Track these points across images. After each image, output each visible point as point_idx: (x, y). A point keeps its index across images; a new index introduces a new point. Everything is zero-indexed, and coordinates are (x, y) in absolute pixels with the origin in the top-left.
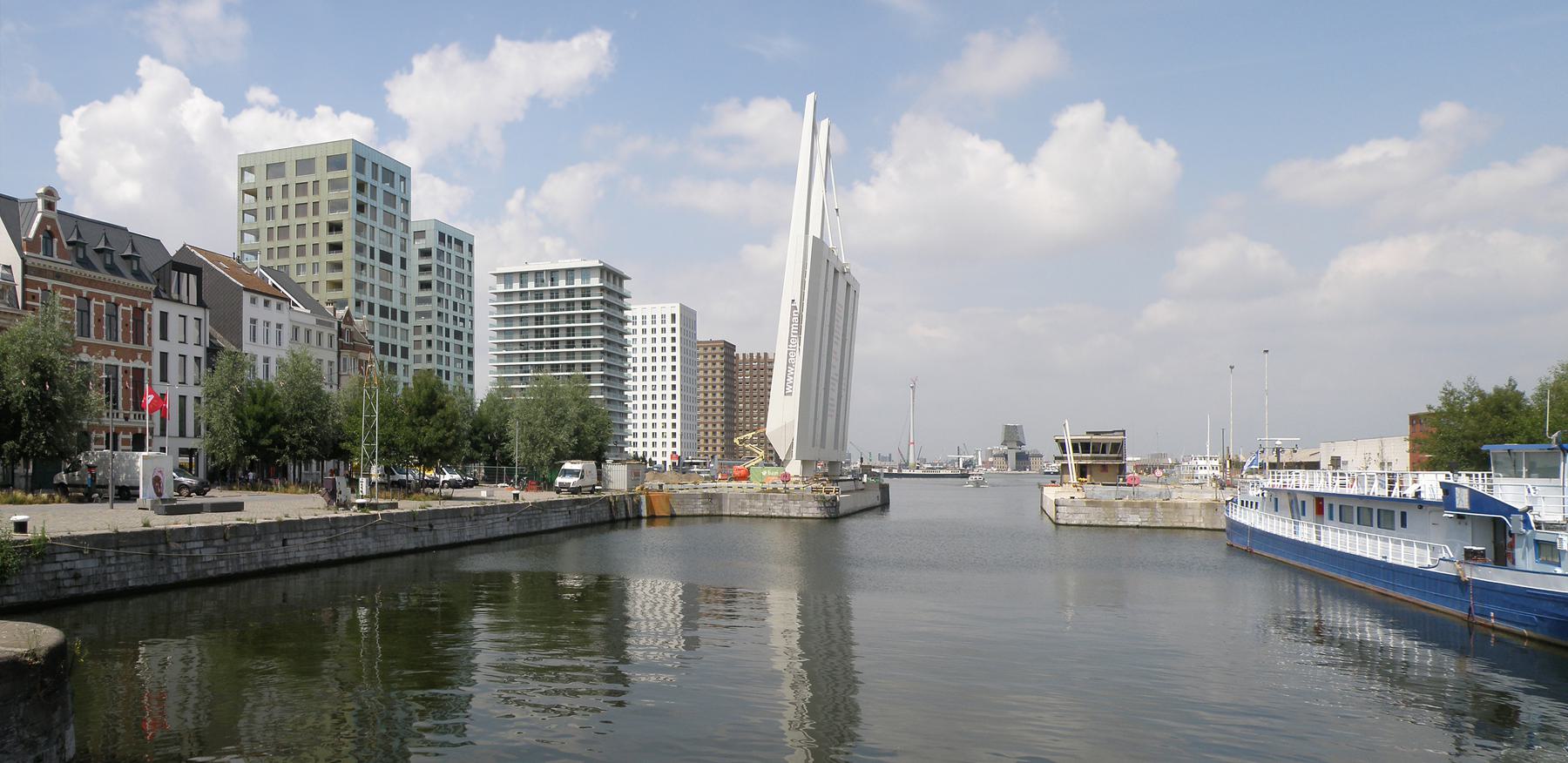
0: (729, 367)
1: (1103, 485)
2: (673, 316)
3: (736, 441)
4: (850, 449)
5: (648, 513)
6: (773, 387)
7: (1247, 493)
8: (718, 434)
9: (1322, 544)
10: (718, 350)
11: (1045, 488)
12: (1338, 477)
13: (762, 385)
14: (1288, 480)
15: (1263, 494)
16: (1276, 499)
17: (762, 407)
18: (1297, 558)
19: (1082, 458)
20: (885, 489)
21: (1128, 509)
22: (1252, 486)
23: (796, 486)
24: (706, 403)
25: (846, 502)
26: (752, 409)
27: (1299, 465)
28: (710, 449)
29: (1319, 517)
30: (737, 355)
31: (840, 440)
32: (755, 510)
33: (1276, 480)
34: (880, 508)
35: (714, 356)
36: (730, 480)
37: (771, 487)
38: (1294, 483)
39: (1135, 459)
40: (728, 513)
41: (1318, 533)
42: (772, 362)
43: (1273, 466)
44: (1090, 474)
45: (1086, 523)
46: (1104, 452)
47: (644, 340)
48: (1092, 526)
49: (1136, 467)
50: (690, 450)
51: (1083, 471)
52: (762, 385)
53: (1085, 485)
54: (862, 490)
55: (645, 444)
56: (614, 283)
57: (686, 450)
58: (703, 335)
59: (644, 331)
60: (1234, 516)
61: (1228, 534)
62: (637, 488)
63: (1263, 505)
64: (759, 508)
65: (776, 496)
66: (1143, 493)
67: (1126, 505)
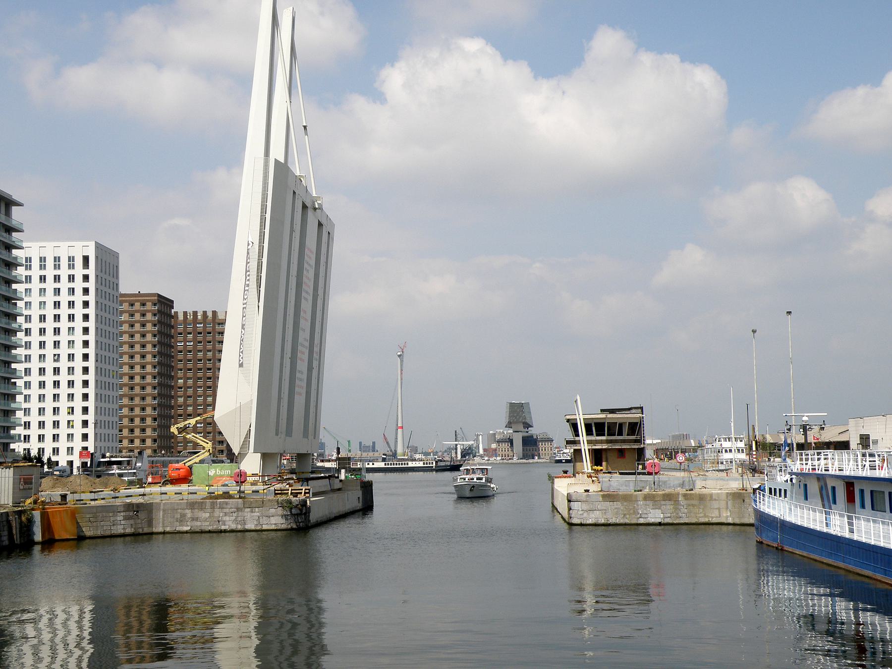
1: (621, 474)
2: (86, 259)
3: (174, 429)
4: (323, 436)
6: (224, 356)
7: (776, 479)
8: (149, 421)
9: (855, 537)
10: (149, 306)
11: (556, 480)
12: (868, 458)
13: (210, 354)
14: (816, 463)
15: (791, 480)
16: (806, 486)
17: (209, 383)
18: (830, 555)
19: (597, 442)
20: (367, 488)
22: (781, 471)
23: (254, 488)
24: (132, 378)
25: (319, 507)
26: (195, 387)
27: (828, 445)
28: (137, 442)
29: (851, 505)
30: (176, 313)
31: (311, 427)
32: (199, 524)
33: (804, 462)
34: (361, 513)
35: (143, 315)
36: (165, 484)
37: (220, 491)
38: (823, 466)
39: (655, 442)
40: (161, 530)
41: (851, 524)
42: (223, 323)
43: (801, 447)
44: (607, 461)
45: (603, 521)
46: (620, 434)
47: (42, 291)
48: (610, 525)
49: (657, 452)
50: (107, 444)
51: (598, 457)
52: (210, 354)
53: (601, 475)
54: (339, 489)
55: (41, 438)
57: (103, 444)
58: (128, 285)
59: (43, 279)
60: (762, 507)
61: (757, 529)
62: (29, 501)
63: (792, 492)
64: (204, 520)
65: (227, 503)
66: (665, 482)
67: (646, 498)
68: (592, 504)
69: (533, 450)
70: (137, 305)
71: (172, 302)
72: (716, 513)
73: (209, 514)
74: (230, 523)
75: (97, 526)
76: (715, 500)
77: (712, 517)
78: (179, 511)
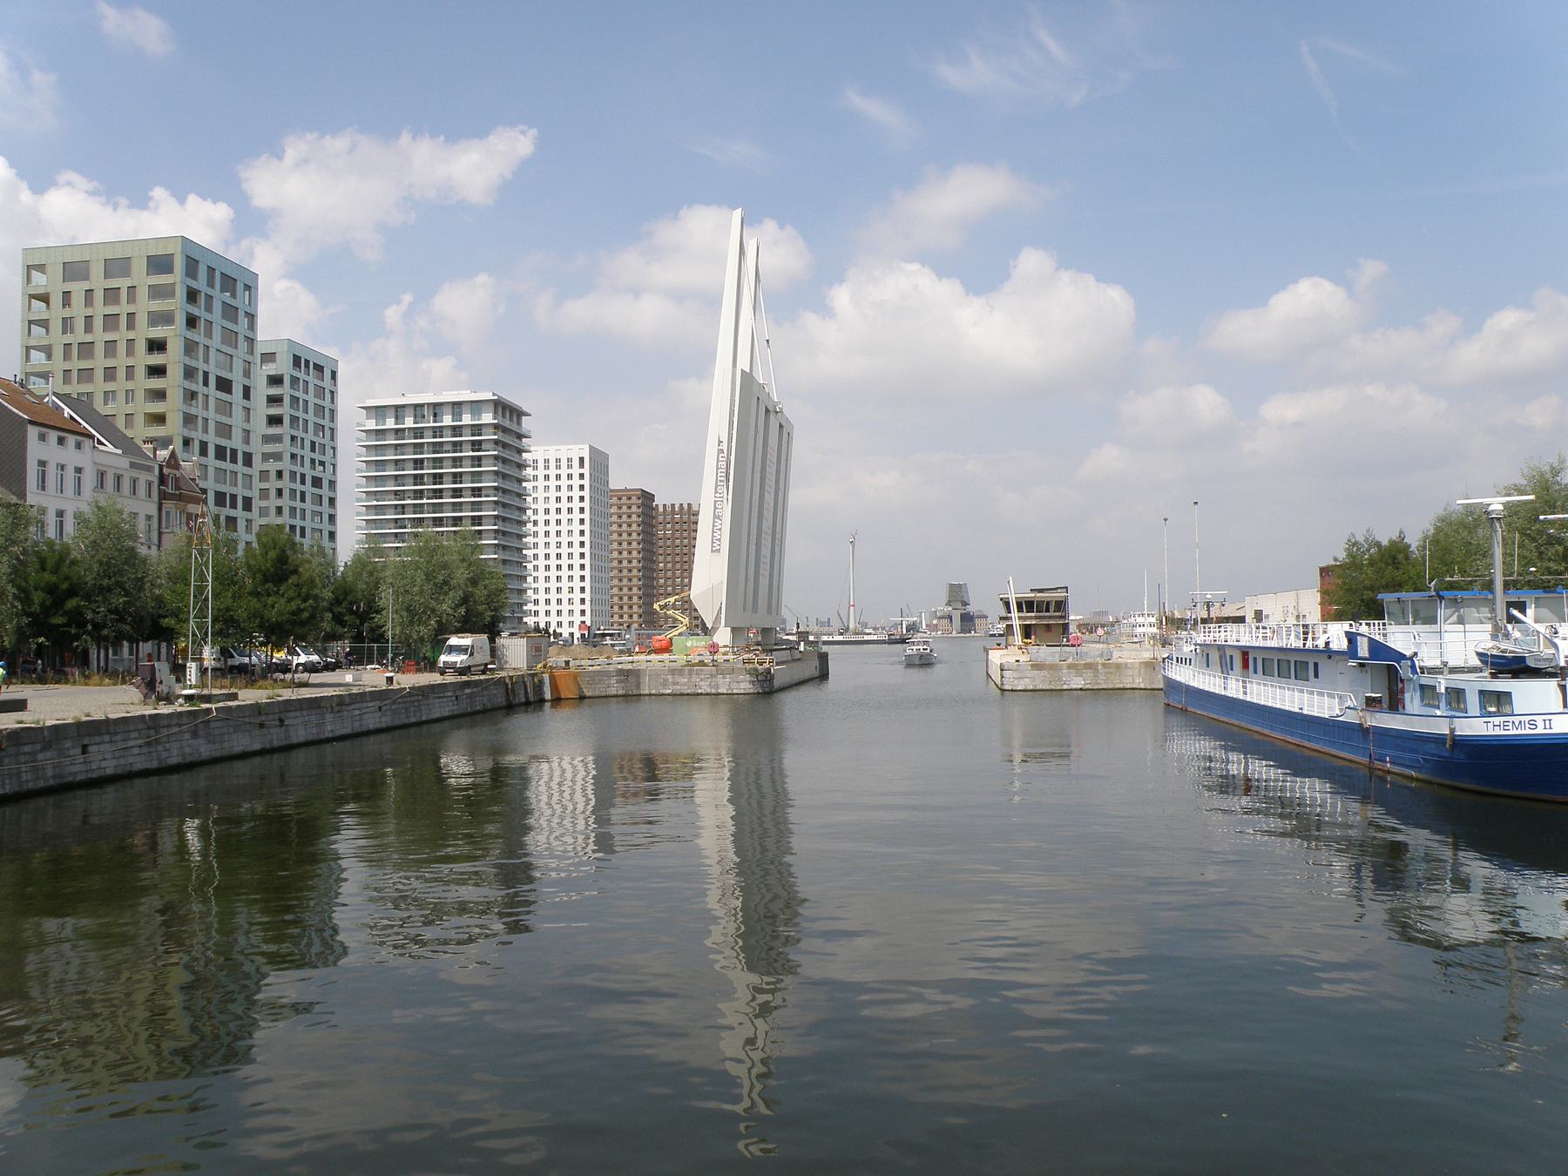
56: (511, 420)
65: (702, 670)
71: (654, 496)
74: (705, 687)
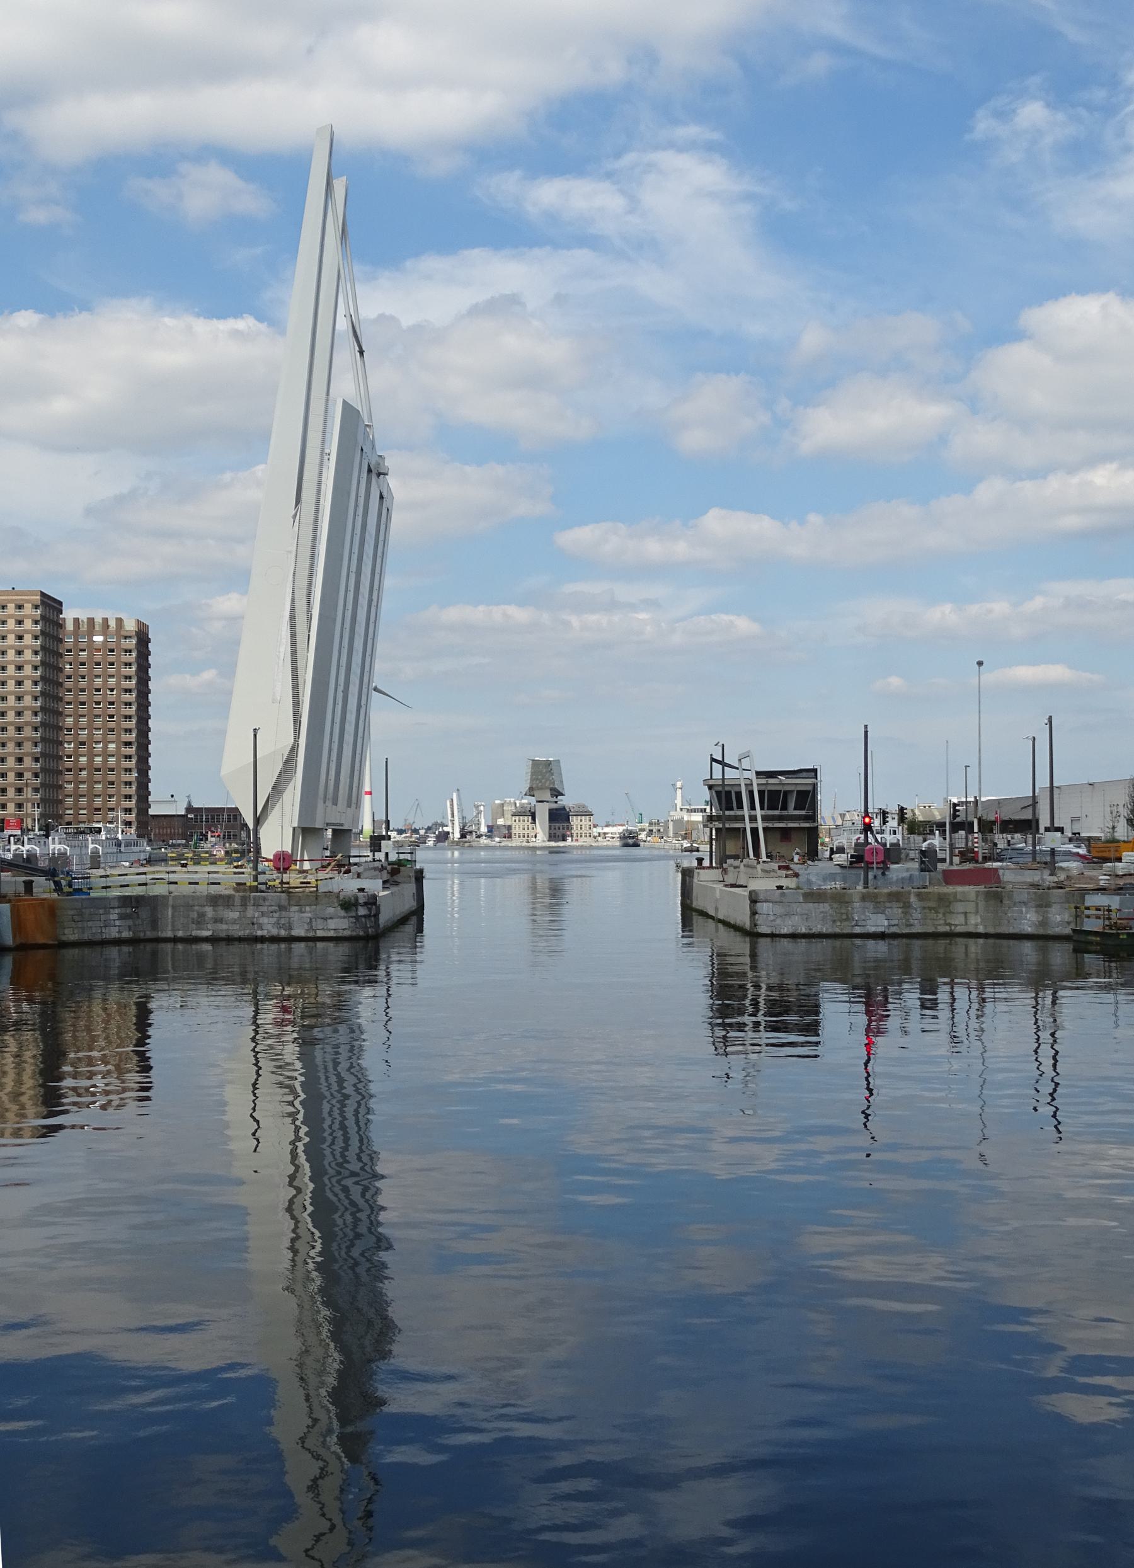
0: (51, 645)
5: (14, 937)
10: (28, 609)
21: (867, 904)
32: (224, 927)
40: (169, 934)
45: (804, 931)
64: (232, 921)
65: (264, 899)
68: (789, 906)
69: (564, 829)
70: (11, 609)
71: (61, 603)
72: (960, 919)
73: (238, 913)
74: (270, 927)
75: (83, 928)
76: (961, 901)
77: (956, 925)
78: (196, 908)
